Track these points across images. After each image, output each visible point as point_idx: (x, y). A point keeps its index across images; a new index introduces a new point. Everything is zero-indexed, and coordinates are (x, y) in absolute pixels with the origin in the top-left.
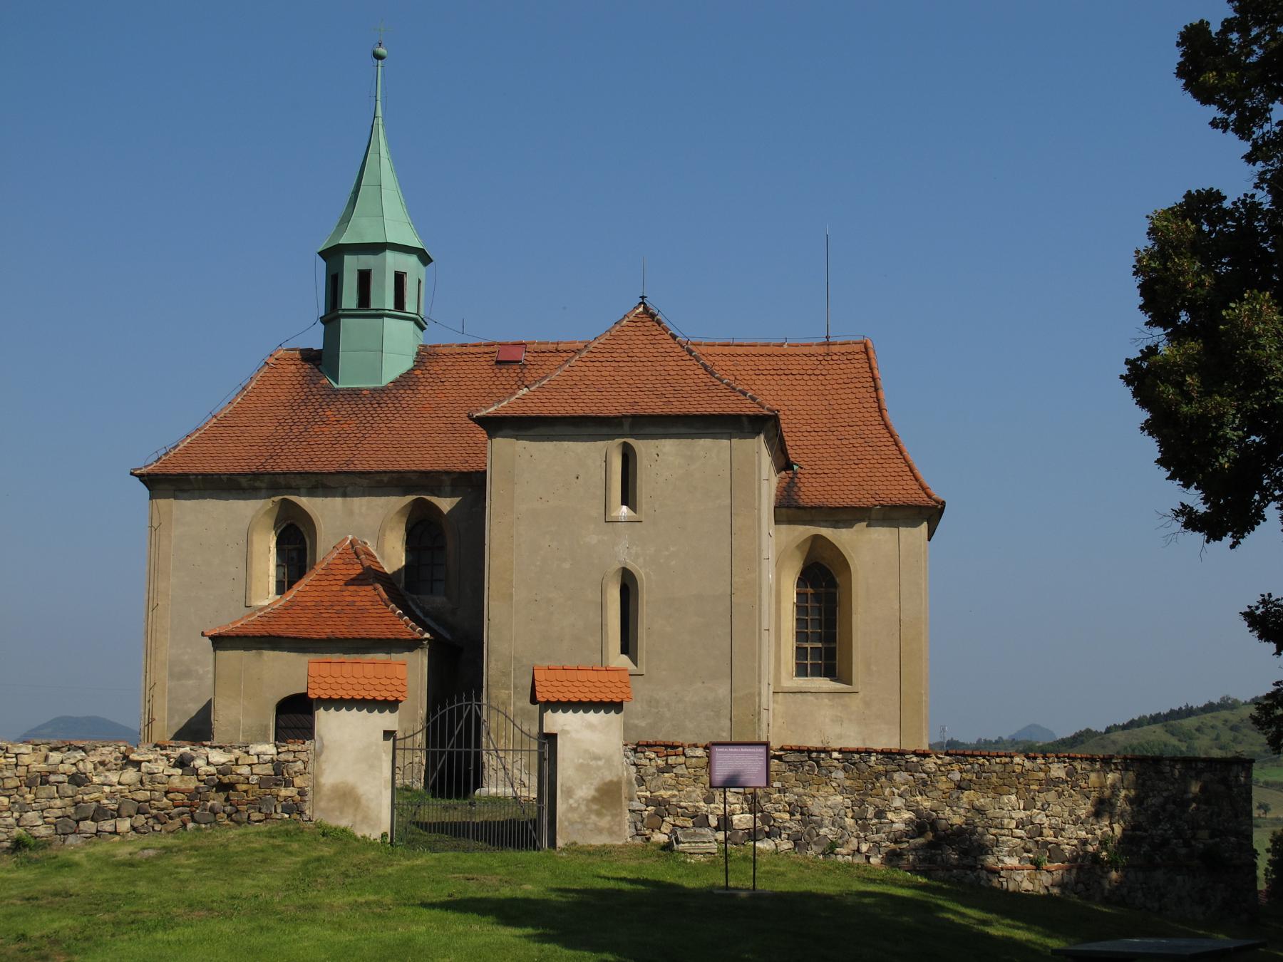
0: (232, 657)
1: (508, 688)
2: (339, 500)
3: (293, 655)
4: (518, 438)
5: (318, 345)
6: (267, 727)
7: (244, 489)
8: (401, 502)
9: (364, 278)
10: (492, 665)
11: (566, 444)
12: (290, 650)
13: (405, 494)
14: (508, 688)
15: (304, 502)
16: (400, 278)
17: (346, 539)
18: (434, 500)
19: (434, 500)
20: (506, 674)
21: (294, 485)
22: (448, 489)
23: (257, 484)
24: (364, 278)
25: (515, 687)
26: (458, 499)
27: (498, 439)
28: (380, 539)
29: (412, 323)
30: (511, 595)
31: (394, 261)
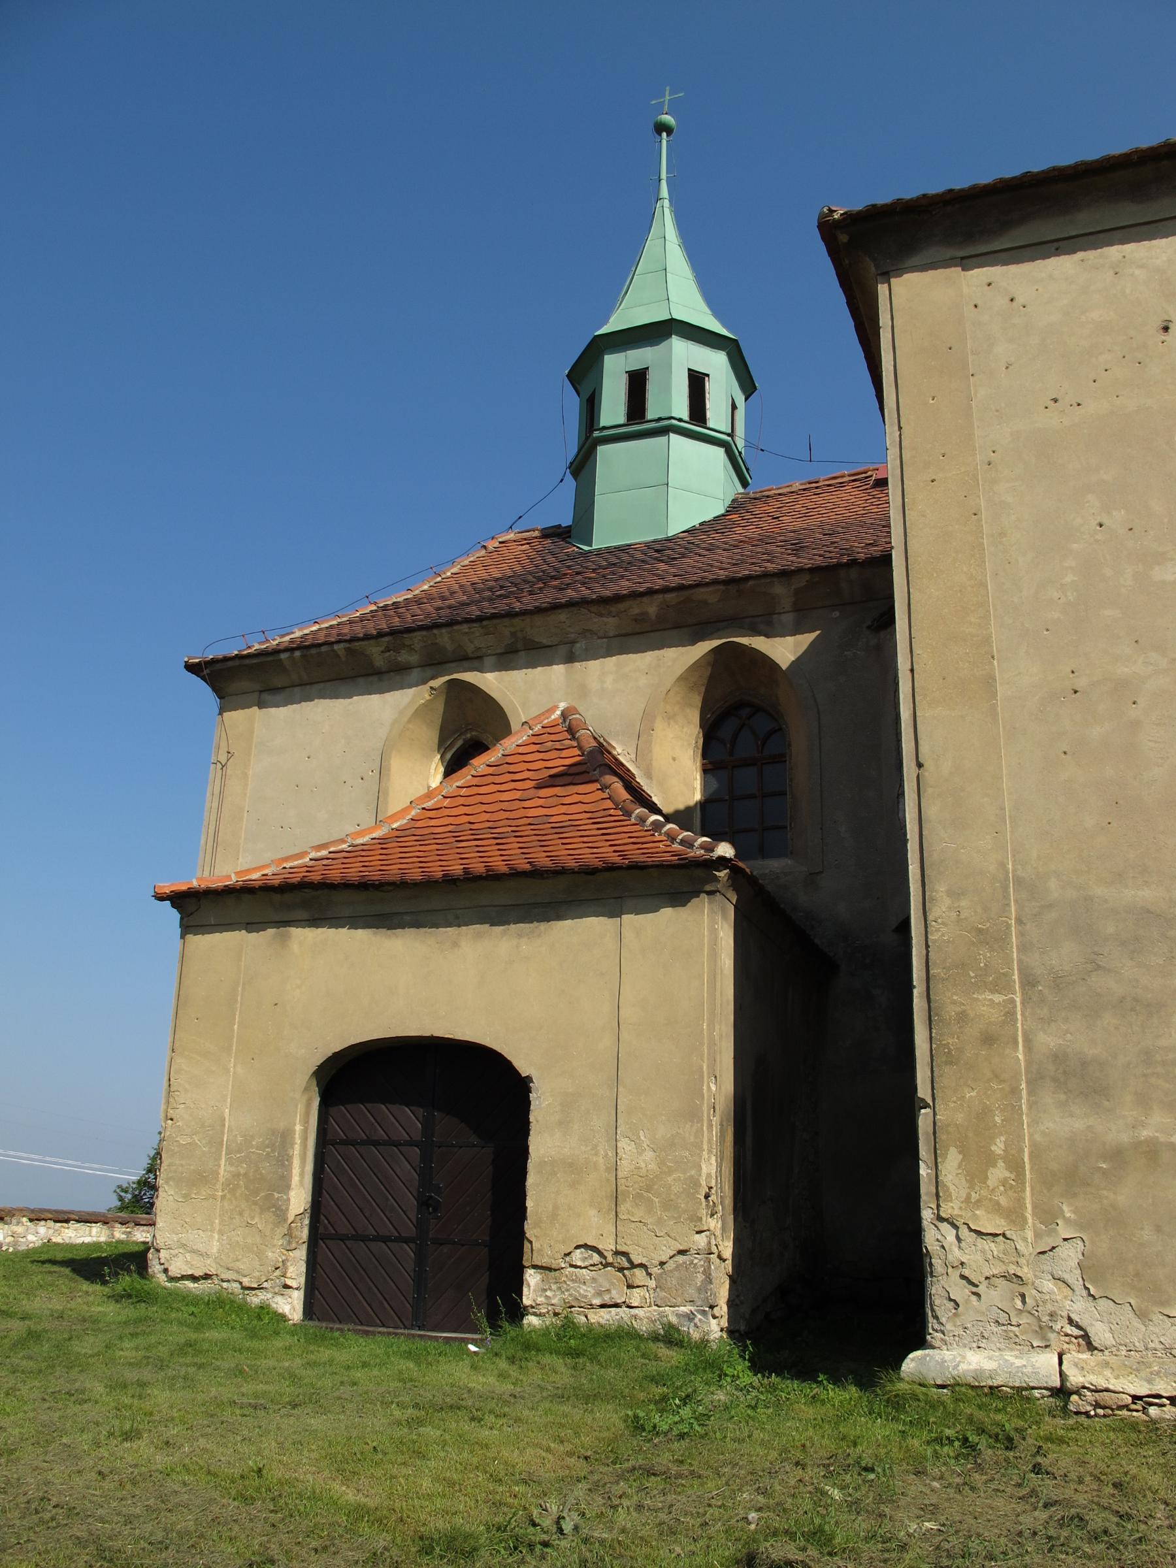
0: (223, 947)
1: (1001, 984)
2: (559, 670)
3: (361, 934)
4: (966, 263)
5: (566, 520)
6: (285, 1138)
7: (379, 673)
8: (682, 658)
9: (637, 382)
10: (941, 909)
11: (1114, 252)
12: (355, 922)
13: (694, 640)
14: (1008, 988)
15: (491, 681)
16: (697, 382)
17: (557, 707)
18: (759, 643)
19: (759, 643)
20: (990, 937)
21: (470, 648)
22: (788, 618)
23: (404, 657)
24: (637, 382)
25: (1029, 982)
26: (810, 637)
27: (909, 277)
28: (643, 736)
29: (720, 452)
30: (989, 683)
31: (684, 355)
